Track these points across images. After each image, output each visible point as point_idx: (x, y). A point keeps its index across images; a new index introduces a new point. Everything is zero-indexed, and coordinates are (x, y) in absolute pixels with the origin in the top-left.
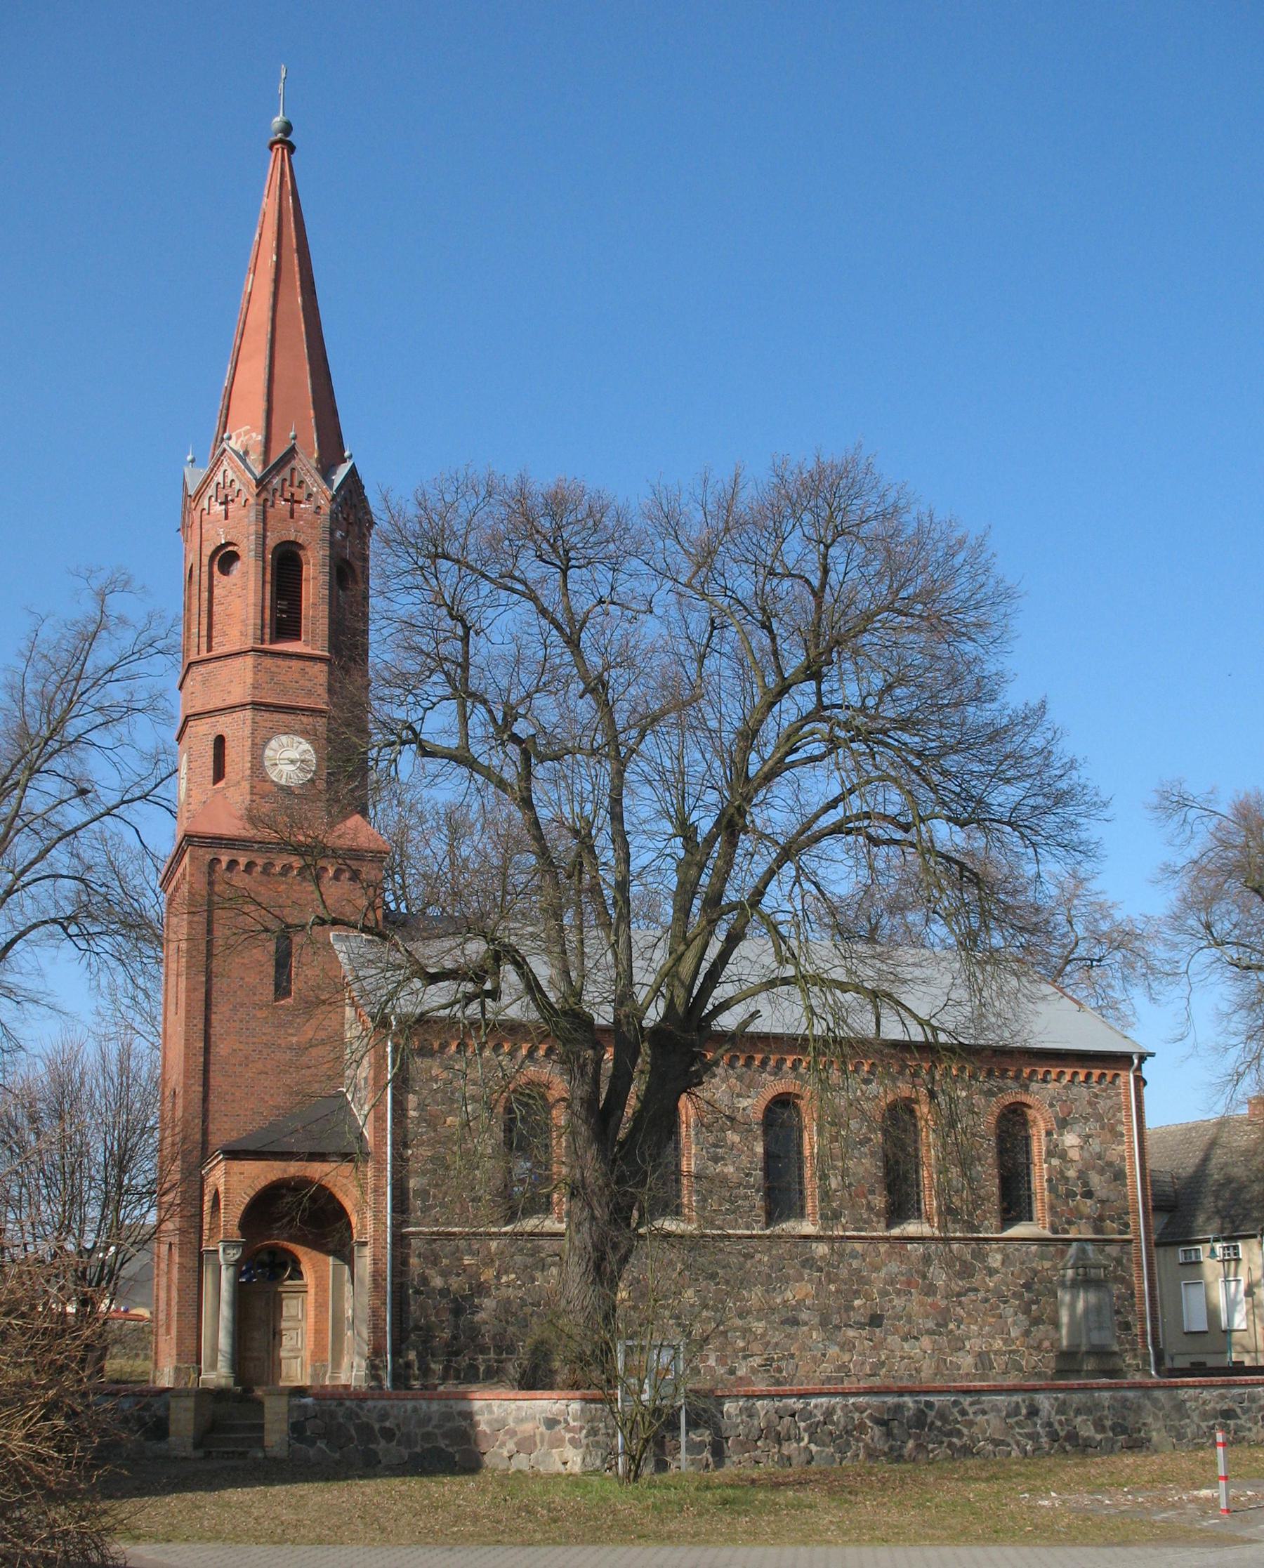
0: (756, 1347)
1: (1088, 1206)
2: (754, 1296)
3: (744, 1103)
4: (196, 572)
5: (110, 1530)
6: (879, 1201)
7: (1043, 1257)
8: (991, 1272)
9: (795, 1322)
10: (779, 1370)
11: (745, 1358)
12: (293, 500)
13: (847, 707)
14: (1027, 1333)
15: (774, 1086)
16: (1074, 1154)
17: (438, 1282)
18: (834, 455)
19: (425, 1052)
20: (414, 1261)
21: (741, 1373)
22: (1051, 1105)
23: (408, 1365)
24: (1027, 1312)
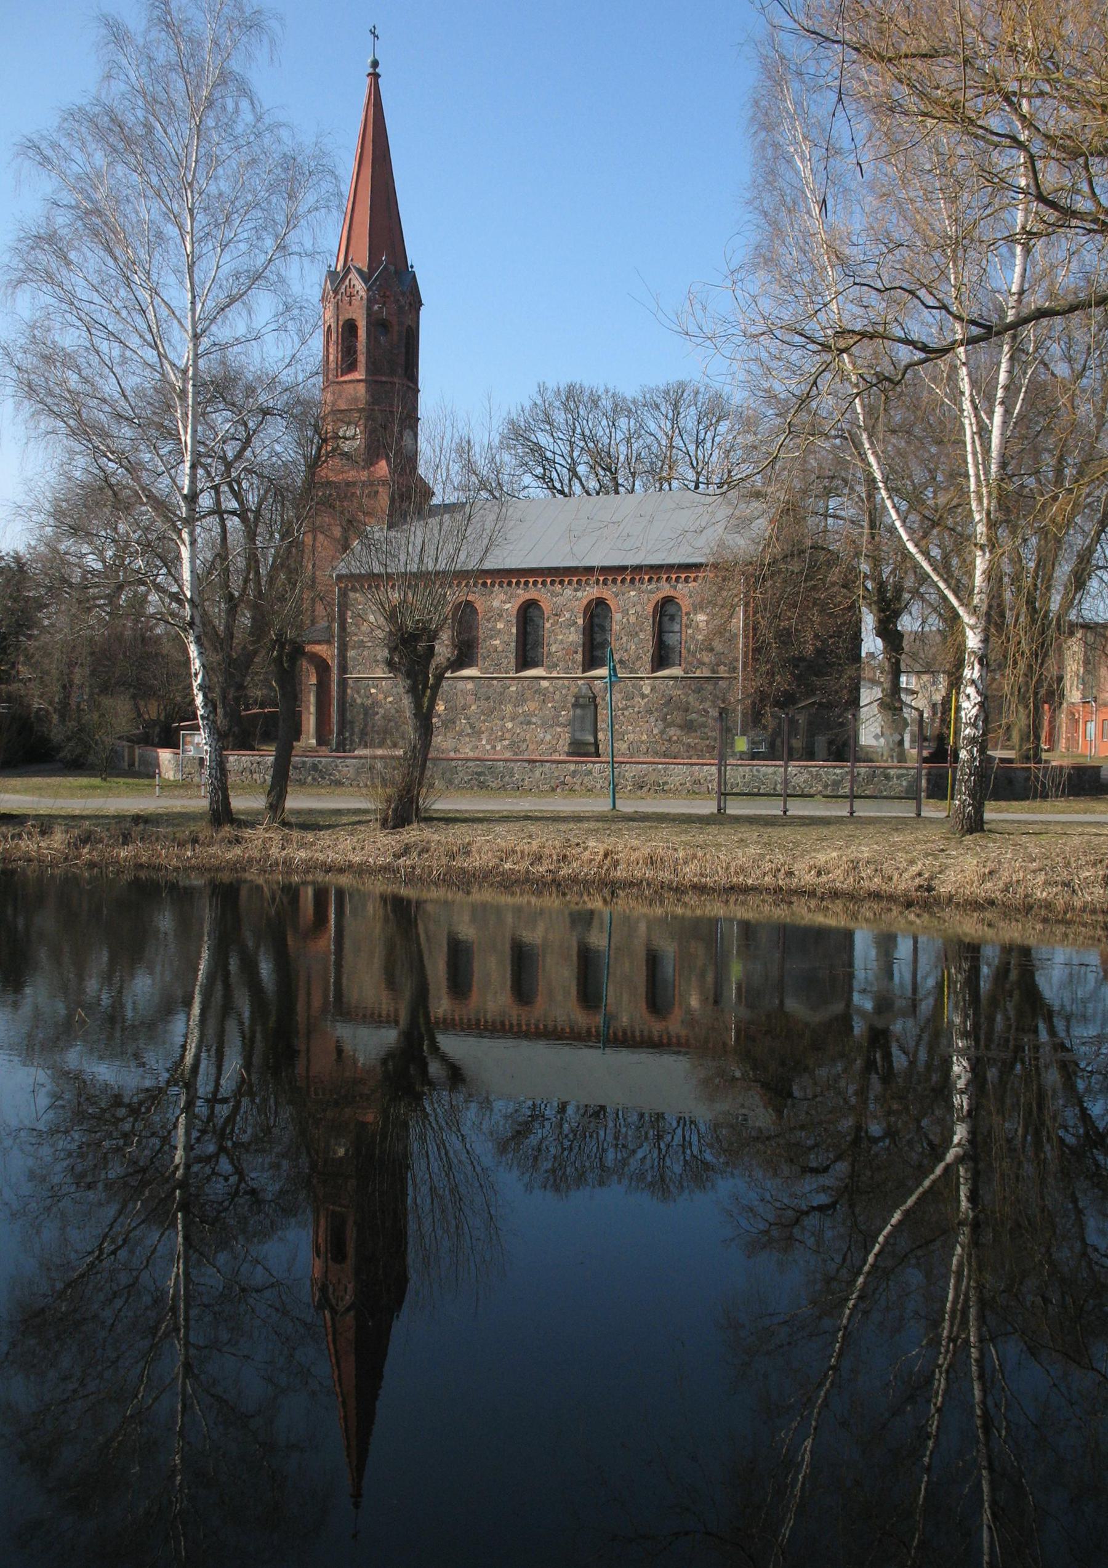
0: (507, 736)
1: (707, 658)
2: (509, 708)
3: (508, 606)
4: (333, 330)
5: (53, 1132)
6: (579, 657)
7: (674, 687)
8: (643, 696)
9: (529, 723)
10: (519, 748)
11: (501, 740)
12: (351, 296)
13: (687, 1534)
14: (662, 732)
15: (523, 595)
16: (702, 625)
17: (359, 701)
18: (20, 1012)
19: (354, 589)
20: (349, 691)
21: (498, 748)
22: (691, 597)
23: (345, 739)
24: (664, 720)
